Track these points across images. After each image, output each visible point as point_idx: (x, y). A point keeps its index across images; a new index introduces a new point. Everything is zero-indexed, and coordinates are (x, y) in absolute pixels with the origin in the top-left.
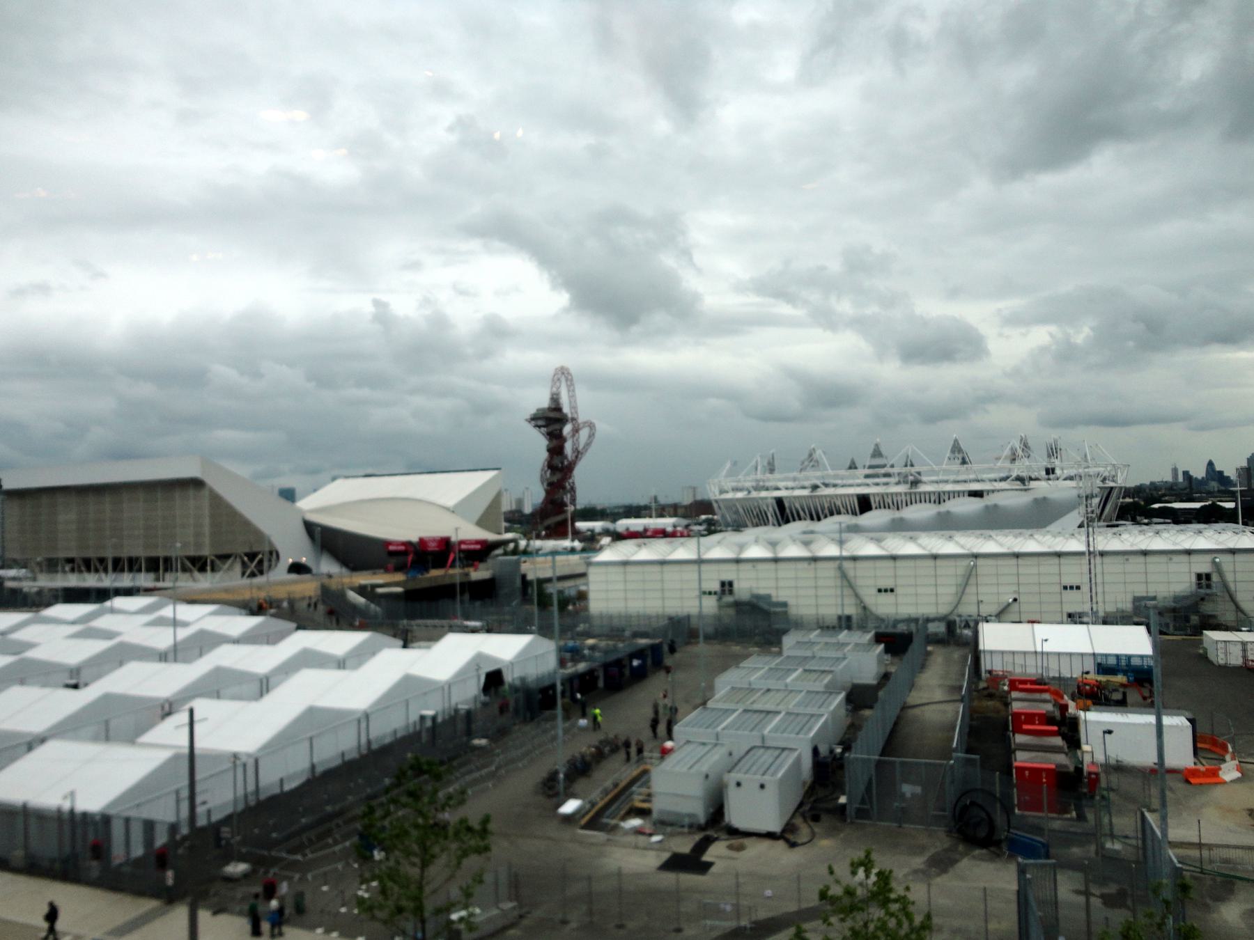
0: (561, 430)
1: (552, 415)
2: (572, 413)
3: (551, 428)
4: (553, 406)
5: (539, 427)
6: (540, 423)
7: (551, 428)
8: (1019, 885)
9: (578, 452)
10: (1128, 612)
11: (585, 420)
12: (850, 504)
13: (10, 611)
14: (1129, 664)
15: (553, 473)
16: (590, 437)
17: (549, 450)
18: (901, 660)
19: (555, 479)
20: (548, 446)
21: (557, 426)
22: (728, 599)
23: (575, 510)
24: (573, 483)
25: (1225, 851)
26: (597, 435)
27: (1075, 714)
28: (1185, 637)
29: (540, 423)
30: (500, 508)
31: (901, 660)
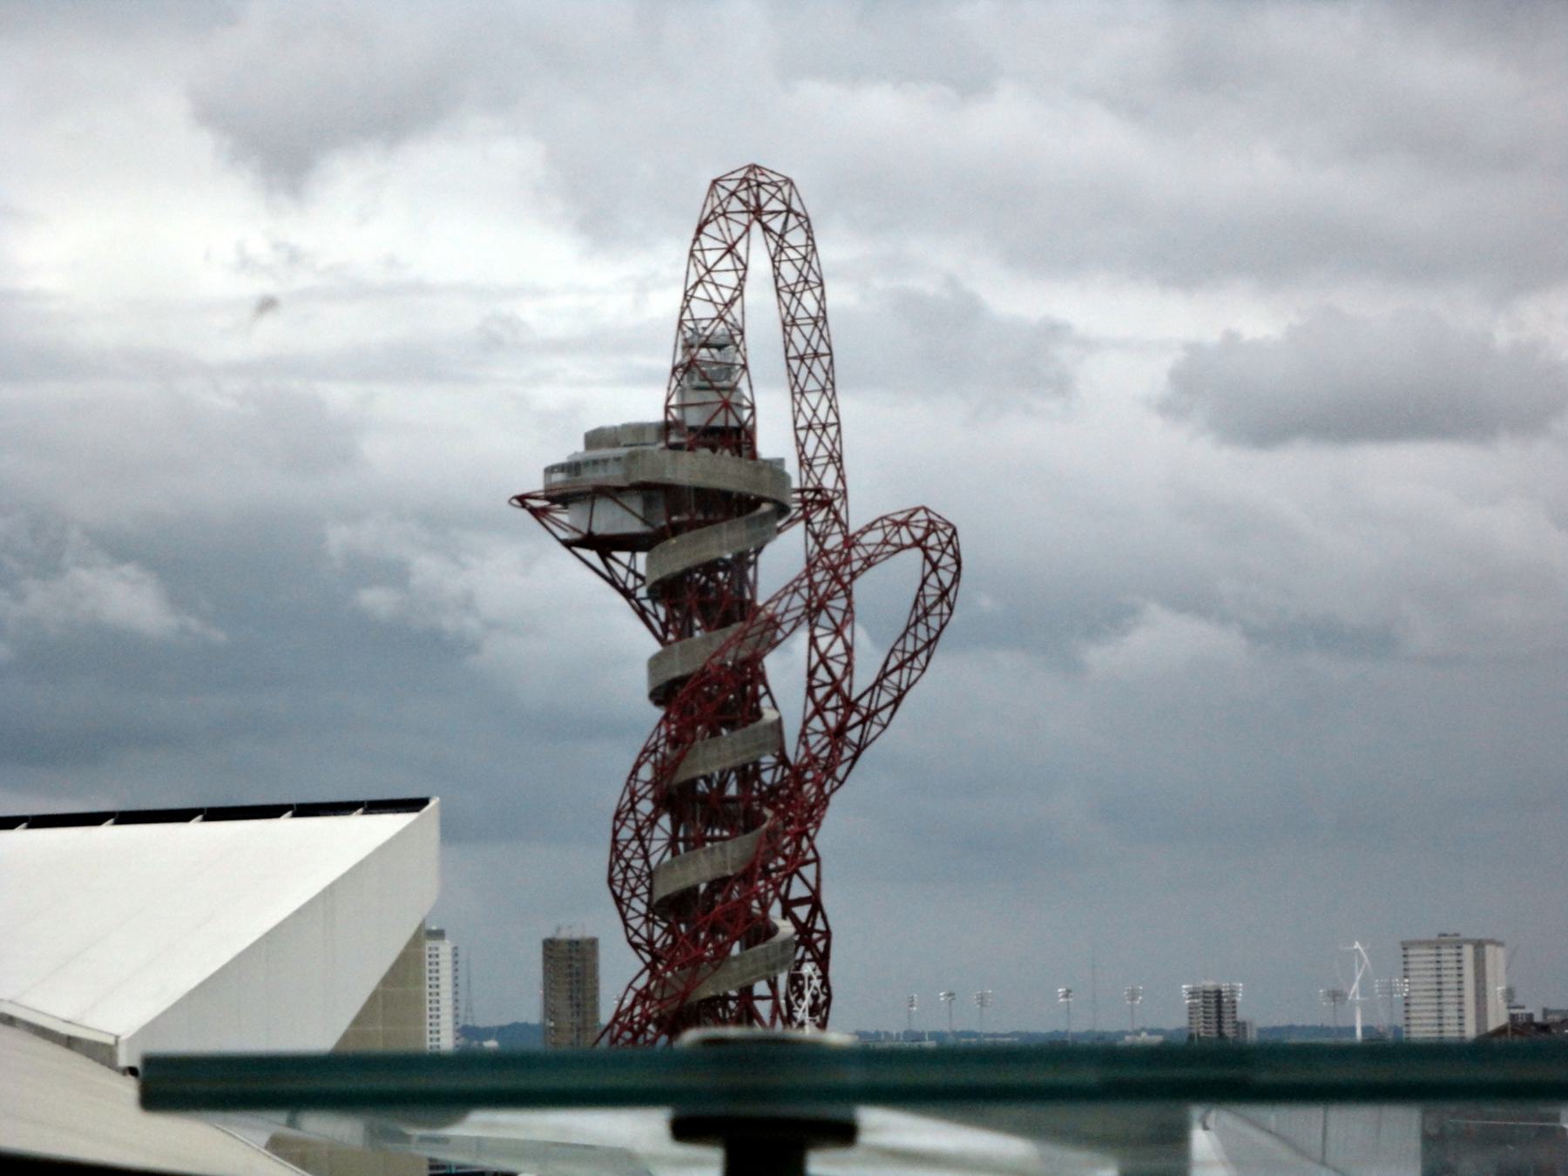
0: (742, 563)
2: (805, 463)
3: (681, 555)
4: (680, 403)
5: (605, 545)
6: (611, 519)
7: (681, 555)
11: (894, 505)
12: (1426, 990)
13: (182, 1111)
15: (686, 842)
16: (920, 613)
17: (663, 694)
18: (1216, 1003)
19: (700, 871)
20: (655, 663)
21: (719, 543)
22: (825, 599)
25: (1227, 1020)
28: (698, 818)
29: (611, 519)
30: (597, 1020)
31: (1216, 1003)
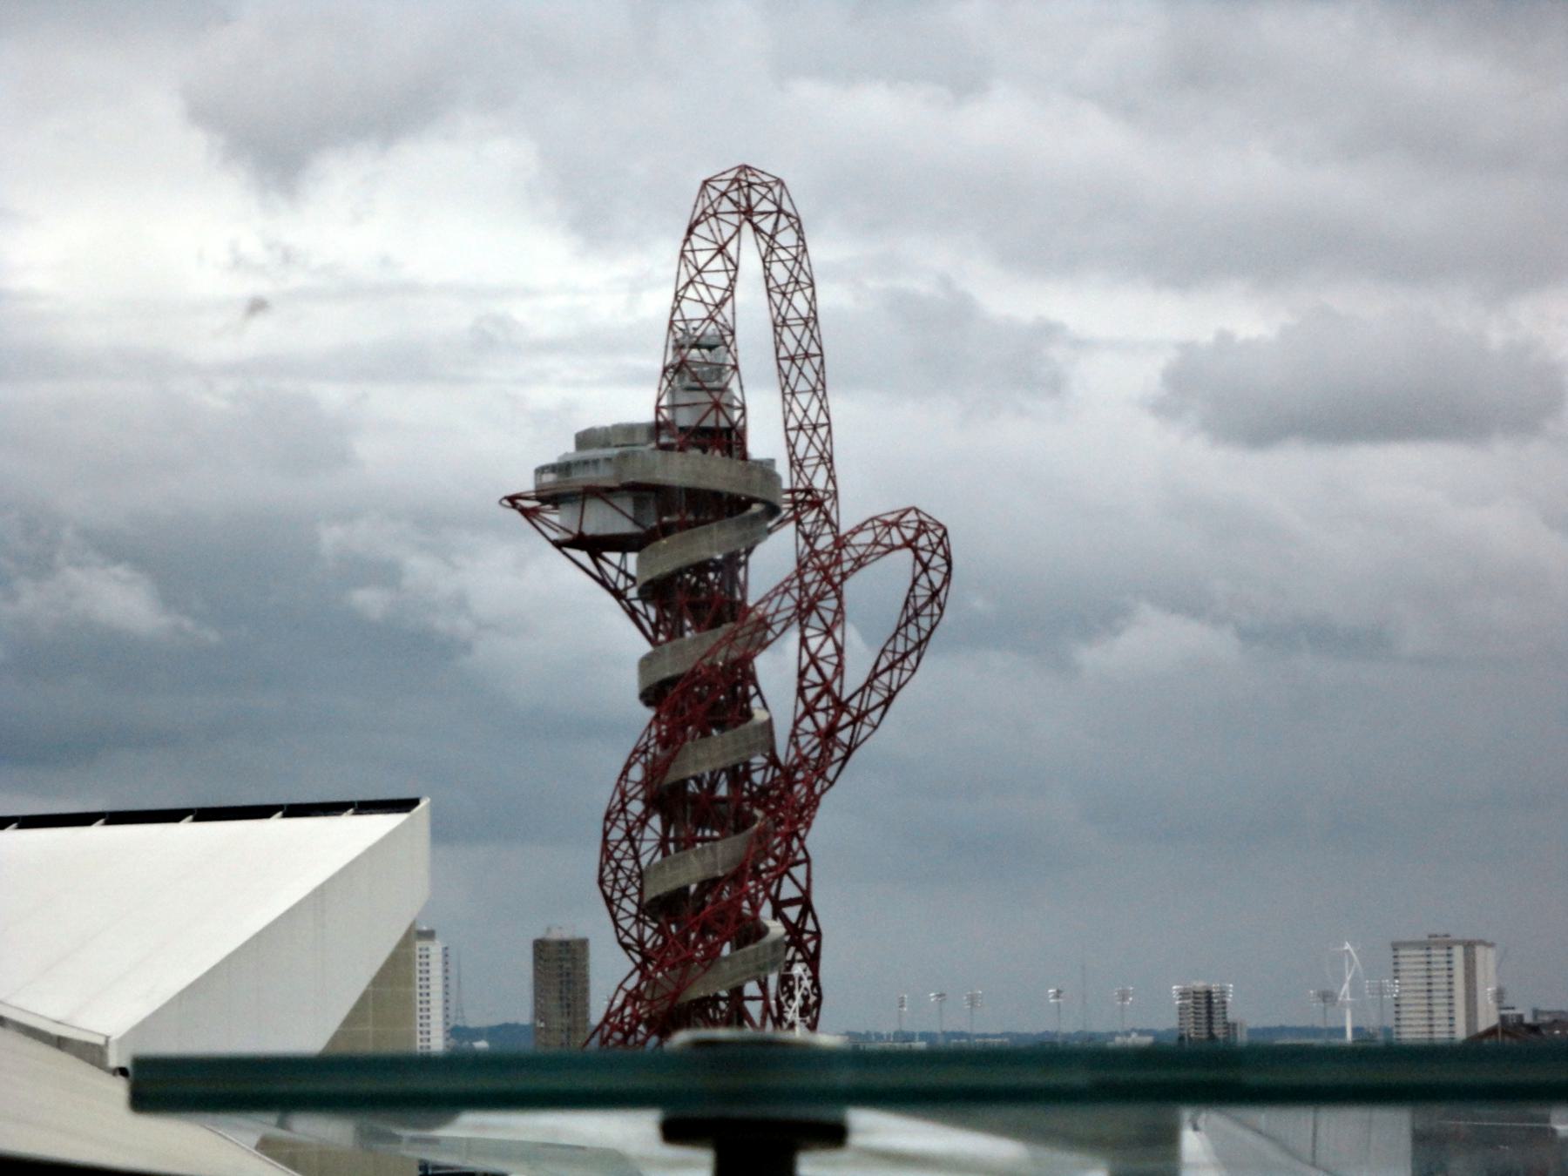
0: (732, 564)
1: (683, 470)
2: (796, 463)
3: (671, 556)
6: (601, 520)
7: (671, 556)
8: (723, 877)
9: (840, 706)
10: (571, 454)
11: (884, 506)
14: (739, 565)
15: (676, 843)
16: (911, 614)
17: (653, 695)
18: (1207, 1003)
19: (690, 871)
21: (710, 544)
23: (727, 1013)
24: (805, 903)
26: (955, 595)
27: (1430, 1039)
29: (601, 520)
31: (1207, 1003)
